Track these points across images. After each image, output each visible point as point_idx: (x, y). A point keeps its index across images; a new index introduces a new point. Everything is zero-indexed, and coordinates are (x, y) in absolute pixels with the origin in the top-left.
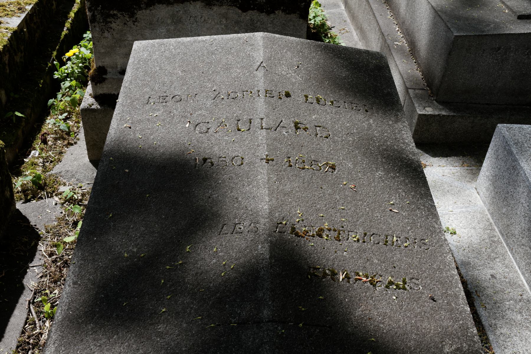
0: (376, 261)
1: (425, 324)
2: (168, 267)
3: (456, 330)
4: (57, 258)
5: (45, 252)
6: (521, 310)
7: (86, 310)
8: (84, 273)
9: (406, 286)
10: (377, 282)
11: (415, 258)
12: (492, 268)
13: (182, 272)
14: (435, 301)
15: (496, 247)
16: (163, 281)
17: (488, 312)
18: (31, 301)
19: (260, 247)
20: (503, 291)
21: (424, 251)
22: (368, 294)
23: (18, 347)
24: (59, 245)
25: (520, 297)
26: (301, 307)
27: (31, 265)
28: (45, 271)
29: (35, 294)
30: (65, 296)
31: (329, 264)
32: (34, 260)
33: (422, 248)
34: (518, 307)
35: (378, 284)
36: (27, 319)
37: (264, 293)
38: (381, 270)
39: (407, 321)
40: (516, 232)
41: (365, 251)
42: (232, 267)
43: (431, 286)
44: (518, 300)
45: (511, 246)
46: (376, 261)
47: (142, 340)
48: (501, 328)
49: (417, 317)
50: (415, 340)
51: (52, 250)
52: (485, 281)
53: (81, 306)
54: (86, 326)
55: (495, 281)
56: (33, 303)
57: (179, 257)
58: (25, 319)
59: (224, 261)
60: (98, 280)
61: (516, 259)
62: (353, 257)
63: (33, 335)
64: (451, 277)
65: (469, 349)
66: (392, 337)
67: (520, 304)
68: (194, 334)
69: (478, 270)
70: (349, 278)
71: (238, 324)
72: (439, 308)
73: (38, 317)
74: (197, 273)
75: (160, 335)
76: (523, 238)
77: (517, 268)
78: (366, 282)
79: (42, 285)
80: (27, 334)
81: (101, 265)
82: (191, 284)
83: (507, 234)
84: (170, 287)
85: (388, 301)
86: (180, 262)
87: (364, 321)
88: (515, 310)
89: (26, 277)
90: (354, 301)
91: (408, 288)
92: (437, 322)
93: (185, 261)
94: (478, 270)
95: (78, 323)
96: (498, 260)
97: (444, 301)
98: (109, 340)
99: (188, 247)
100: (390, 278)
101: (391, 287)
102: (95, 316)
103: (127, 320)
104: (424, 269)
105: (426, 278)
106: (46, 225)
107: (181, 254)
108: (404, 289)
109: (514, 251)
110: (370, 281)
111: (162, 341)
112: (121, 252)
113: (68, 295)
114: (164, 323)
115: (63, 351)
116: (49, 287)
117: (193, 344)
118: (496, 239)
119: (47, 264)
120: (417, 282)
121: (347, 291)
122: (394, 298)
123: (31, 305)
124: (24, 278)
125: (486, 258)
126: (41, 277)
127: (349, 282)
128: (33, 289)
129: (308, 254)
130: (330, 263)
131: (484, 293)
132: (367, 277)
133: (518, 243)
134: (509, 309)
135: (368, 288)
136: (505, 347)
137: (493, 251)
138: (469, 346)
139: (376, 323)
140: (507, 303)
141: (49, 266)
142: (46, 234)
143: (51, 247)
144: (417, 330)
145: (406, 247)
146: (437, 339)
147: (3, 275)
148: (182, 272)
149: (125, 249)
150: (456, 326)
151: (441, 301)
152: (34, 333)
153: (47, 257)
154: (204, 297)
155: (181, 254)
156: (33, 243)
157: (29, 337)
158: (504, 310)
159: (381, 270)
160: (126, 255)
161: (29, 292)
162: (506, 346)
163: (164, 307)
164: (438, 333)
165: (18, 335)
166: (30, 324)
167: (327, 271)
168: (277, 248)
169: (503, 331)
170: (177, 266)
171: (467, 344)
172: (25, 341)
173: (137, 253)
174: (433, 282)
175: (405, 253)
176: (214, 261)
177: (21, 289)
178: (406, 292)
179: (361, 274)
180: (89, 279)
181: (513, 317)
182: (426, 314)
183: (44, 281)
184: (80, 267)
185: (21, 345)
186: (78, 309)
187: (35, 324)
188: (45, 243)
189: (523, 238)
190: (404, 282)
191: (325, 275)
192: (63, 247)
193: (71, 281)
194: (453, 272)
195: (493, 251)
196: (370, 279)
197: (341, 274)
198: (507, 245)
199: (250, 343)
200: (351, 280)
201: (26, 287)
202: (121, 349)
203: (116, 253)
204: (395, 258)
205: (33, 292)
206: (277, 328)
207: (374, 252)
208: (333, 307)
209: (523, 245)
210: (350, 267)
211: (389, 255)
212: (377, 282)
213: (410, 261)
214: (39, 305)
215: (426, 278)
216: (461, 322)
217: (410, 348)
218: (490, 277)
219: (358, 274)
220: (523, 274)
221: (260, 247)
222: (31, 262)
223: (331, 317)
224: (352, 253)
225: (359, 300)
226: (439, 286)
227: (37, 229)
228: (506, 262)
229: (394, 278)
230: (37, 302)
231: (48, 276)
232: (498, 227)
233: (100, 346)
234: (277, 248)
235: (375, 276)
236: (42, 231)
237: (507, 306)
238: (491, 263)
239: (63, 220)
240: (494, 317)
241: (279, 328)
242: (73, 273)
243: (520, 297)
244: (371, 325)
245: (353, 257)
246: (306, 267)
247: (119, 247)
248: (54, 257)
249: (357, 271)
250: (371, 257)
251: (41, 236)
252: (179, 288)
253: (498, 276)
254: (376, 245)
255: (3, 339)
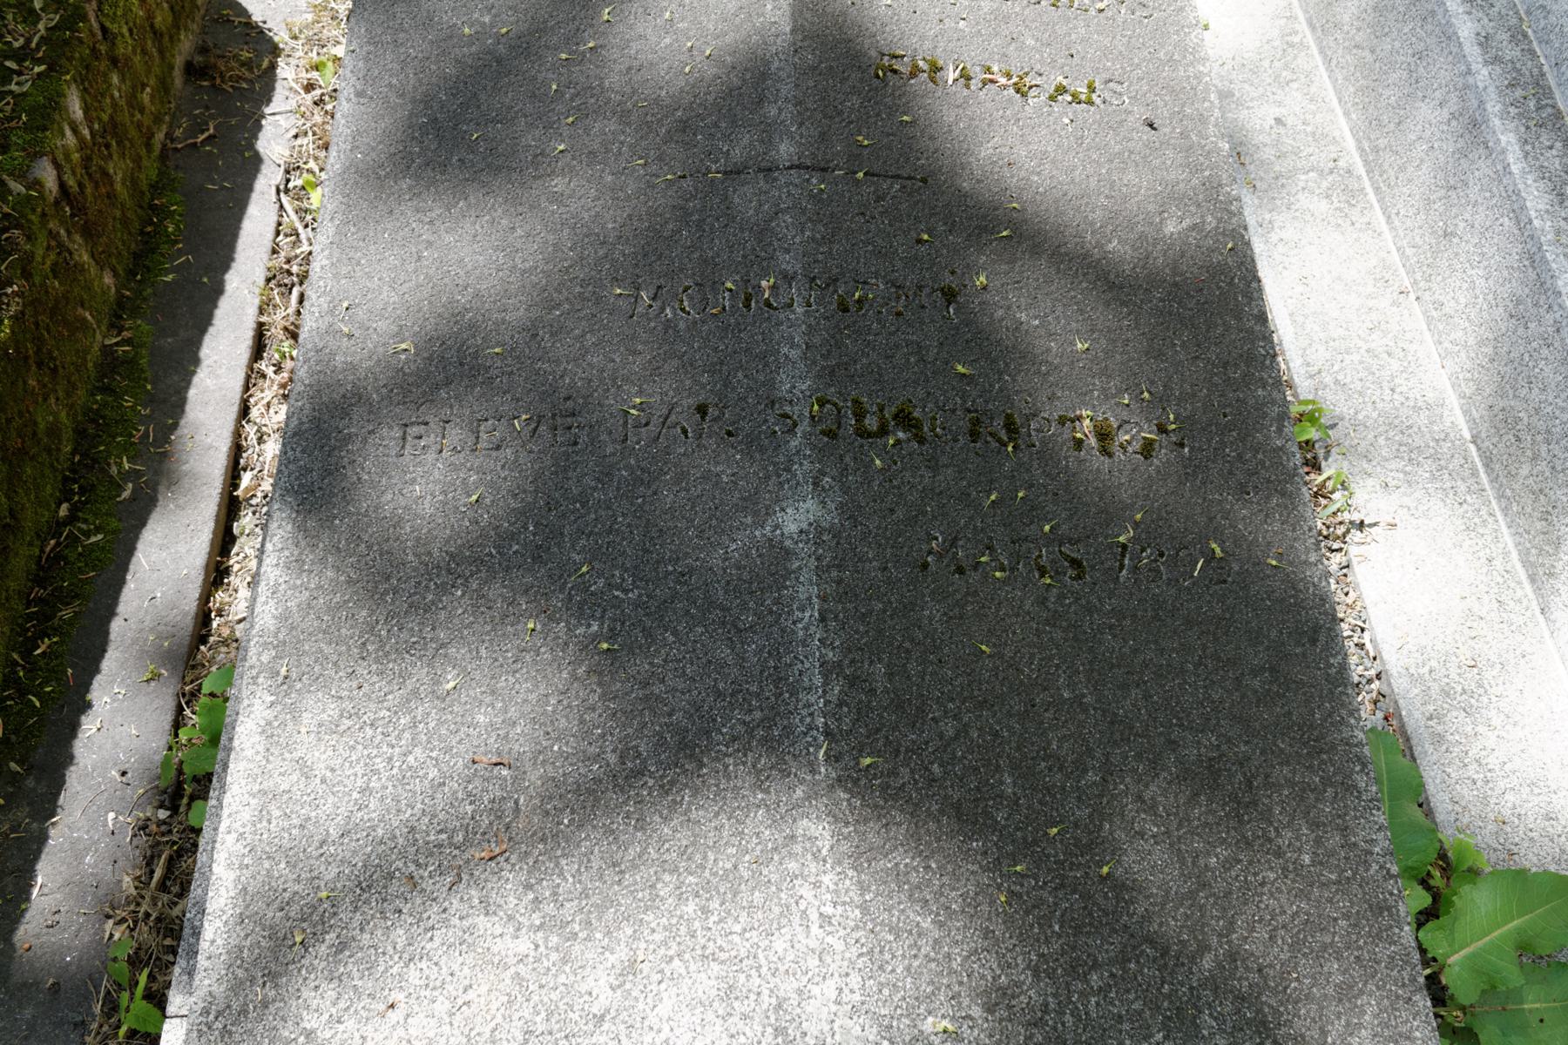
0: (1030, 42)
1: (1130, 176)
2: (564, 56)
3: (1195, 189)
4: (323, 95)
5: (296, 81)
6: (1330, 192)
7: (392, 150)
8: (377, 72)
9: (1094, 96)
10: (1031, 87)
11: (1119, 37)
12: (1280, 104)
13: (597, 67)
14: (1155, 129)
15: (1295, 58)
16: (554, 87)
17: (1259, 198)
18: (282, 187)
19: (769, 7)
20: (1296, 153)
21: (1140, 22)
22: (1008, 112)
23: (268, 280)
24: (323, 64)
25: (1331, 165)
26: (860, 138)
27: (267, 110)
28: (300, 123)
29: (288, 172)
30: (343, 122)
31: (925, 47)
32: (274, 99)
33: (1138, 13)
34: (1325, 184)
35: (1033, 92)
36: (280, 224)
37: (779, 109)
38: (1042, 61)
39: (1090, 170)
40: (1346, 18)
41: (1006, 19)
42: (708, 53)
43: (1150, 97)
44: (1327, 170)
45: (1329, 53)
46: (1030, 42)
47: (520, 209)
48: (1281, 228)
49: (1112, 161)
50: (1104, 208)
51: (309, 76)
52: (1261, 131)
53: (380, 142)
54: (396, 182)
55: (1282, 130)
56: (287, 191)
57: (586, 34)
58: (274, 225)
59: (689, 39)
60: (410, 87)
61: (1334, 82)
62: (979, 31)
63: (296, 257)
64: (1196, 77)
65: (1217, 228)
66: (1056, 201)
67: (1330, 178)
68: (629, 196)
69: (1248, 108)
70: (969, 79)
71: (725, 173)
72: (1162, 143)
73: (302, 219)
74: (630, 68)
75: (557, 198)
76: (1359, 29)
77: (1335, 102)
78: (1005, 87)
79: (300, 152)
80: (283, 254)
81: (414, 54)
82: (617, 92)
83: (1323, 25)
84: (572, 100)
85: (1052, 127)
86: (591, 45)
87: (997, 169)
88: (1317, 192)
89: (261, 135)
90: (977, 127)
91: (1098, 101)
92: (1156, 171)
93: (601, 42)
94: (1248, 108)
95: (379, 178)
96: (1295, 85)
97: (1174, 128)
98: (449, 211)
99: (607, 11)
100: (1060, 78)
101: (1060, 98)
102: (413, 161)
103: (483, 170)
104: (1136, 61)
105: (1140, 79)
106: (289, 20)
107: (592, 26)
108: (1090, 103)
109: (1334, 62)
110: (1015, 84)
111: (562, 210)
112: (455, 25)
113: (349, 119)
114: (564, 176)
115: (353, 234)
116: (316, 159)
117: (629, 216)
118: (1296, 39)
119: (302, 109)
120: (1119, 88)
121: (963, 105)
122: (1067, 121)
123: (282, 195)
124: (257, 139)
125: (1269, 80)
126: (296, 137)
127: (968, 86)
128: (282, 163)
129: (878, 24)
130: (928, 45)
131: (1256, 157)
132: (1009, 76)
133: (1347, 44)
134: (1304, 189)
135: (1010, 100)
136: (1285, 268)
137: (1286, 67)
138: (1220, 220)
139: (1023, 174)
140: (1303, 177)
141: (308, 113)
142: (292, 43)
143: (307, 71)
144: (1112, 188)
145: (1101, 11)
146: (1151, 207)
147: (212, 131)
148: (597, 67)
149: (465, 19)
150: (1195, 181)
151: (1167, 130)
152: (298, 251)
153: (302, 92)
154: (649, 118)
155: (592, 26)
156: (265, 64)
157: (288, 261)
158: (1293, 192)
159: (1042, 61)
160: (467, 30)
161: (274, 166)
162: (1287, 265)
163: (563, 141)
164: (1156, 196)
165: (265, 257)
166: (286, 235)
167: (921, 63)
168: (808, 9)
169: (1288, 234)
170: (584, 52)
171: (1216, 218)
172: (281, 268)
173: (492, 26)
174: (1157, 89)
175: (1098, 24)
176: (668, 41)
177: (254, 163)
178: (1092, 109)
179: (995, 69)
180: (390, 85)
181: (1311, 207)
182: (1133, 156)
183: (301, 146)
184: (367, 60)
185: (275, 276)
186: (373, 149)
187: (298, 235)
188: (293, 61)
189: (1359, 29)
190: (1091, 88)
191: (915, 72)
192: (332, 70)
193: (352, 90)
194: (1202, 69)
195: (1286, 67)
196: (1015, 79)
197: (951, 69)
198: (1322, 51)
199: (751, 212)
200: (973, 82)
201: (265, 157)
202: (477, 227)
203: (445, 26)
204: (1073, 36)
205: (282, 168)
206: (808, 180)
207: (1027, 23)
208: (932, 138)
209: (1356, 46)
210: (972, 57)
211: (1061, 29)
212: (1031, 87)
213: (1107, 42)
214: (301, 194)
215: (1140, 79)
216: (1207, 173)
217: (1092, 224)
218: (1273, 122)
219: (988, 70)
220: (1347, 114)
221: (769, 7)
222: (268, 105)
223: (927, 159)
224: (977, 24)
225: (989, 125)
226: (1167, 98)
227: (270, 30)
228: (1313, 89)
229: (1069, 80)
230: (295, 187)
231: (310, 134)
232: (1306, 12)
233: (431, 222)
234: (808, 9)
235: (1027, 74)
236: (281, 36)
237: (1301, 184)
238: (1279, 91)
239: (325, 8)
240: (1270, 207)
241: (814, 181)
242: (352, 72)
243: (1331, 165)
244: (1012, 177)
245: (979, 31)
246: (873, 53)
247: (450, 14)
248: (318, 92)
249: (988, 63)
250: (1020, 32)
251: (281, 46)
252: (593, 101)
253: (1290, 121)
254: (1032, 7)
255: (234, 265)
